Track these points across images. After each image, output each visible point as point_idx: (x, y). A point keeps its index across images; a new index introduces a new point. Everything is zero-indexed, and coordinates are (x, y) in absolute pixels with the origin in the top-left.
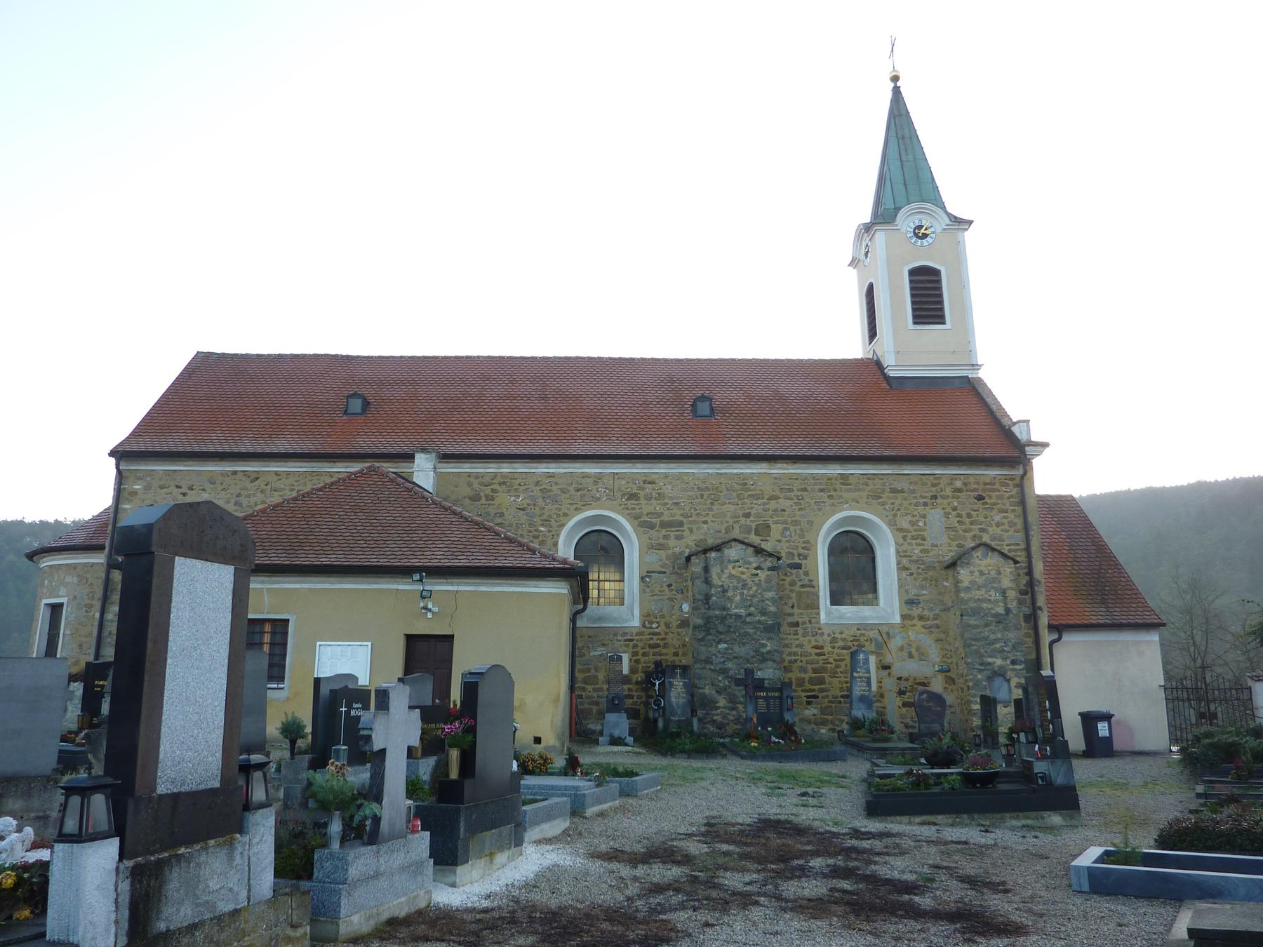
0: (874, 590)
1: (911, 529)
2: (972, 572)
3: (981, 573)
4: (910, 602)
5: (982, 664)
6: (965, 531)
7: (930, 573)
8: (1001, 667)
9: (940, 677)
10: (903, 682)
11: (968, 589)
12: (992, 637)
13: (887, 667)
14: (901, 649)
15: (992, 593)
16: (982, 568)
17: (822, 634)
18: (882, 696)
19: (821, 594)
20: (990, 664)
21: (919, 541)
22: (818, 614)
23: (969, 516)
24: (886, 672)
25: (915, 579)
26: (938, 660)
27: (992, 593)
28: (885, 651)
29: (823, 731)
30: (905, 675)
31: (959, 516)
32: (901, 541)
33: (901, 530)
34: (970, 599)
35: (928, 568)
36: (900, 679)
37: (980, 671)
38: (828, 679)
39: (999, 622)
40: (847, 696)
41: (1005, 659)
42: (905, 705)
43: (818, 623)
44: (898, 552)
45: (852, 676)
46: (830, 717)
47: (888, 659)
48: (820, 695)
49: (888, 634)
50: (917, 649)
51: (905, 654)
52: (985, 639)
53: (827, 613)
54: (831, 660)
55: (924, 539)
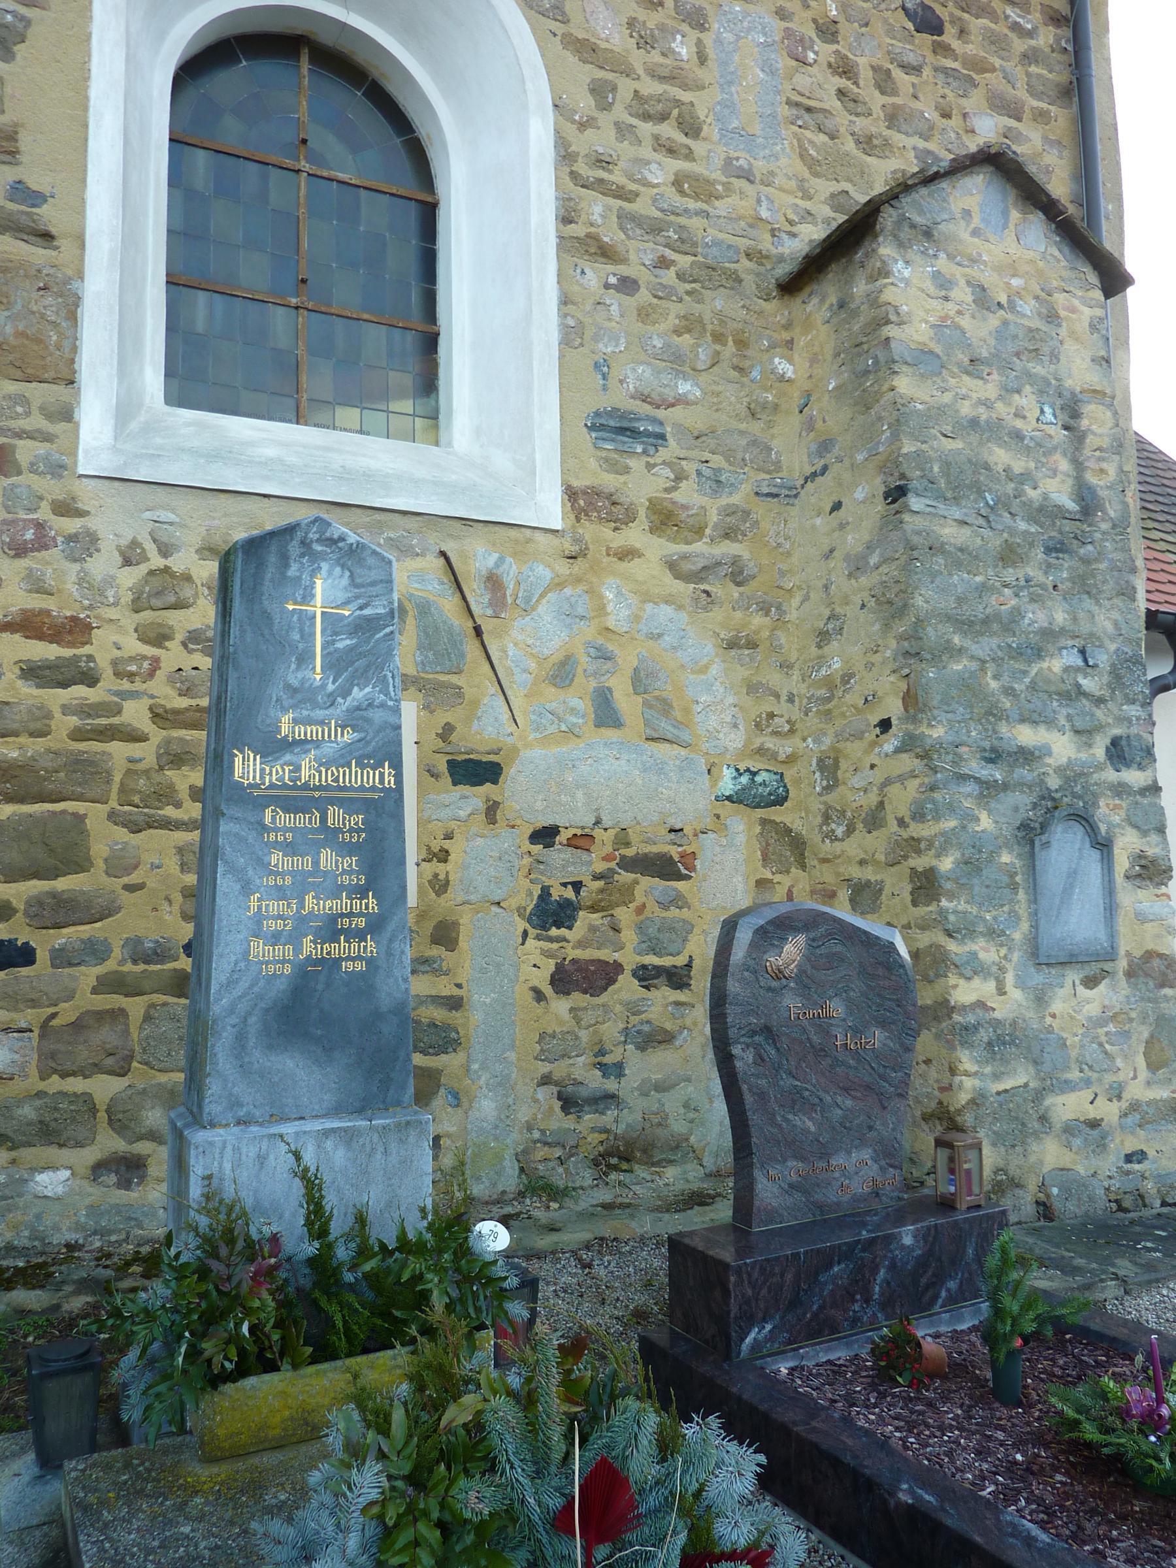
0: (428, 383)
1: (638, 59)
2: (943, 283)
3: (983, 299)
4: (619, 429)
5: (993, 756)
6: (867, 143)
7: (718, 302)
8: (1073, 775)
9: (742, 827)
10: (559, 855)
11: (927, 361)
12: (1035, 617)
13: (477, 771)
14: (561, 673)
15: (1027, 400)
16: (988, 277)
17: (83, 545)
18: (445, 934)
19: (98, 287)
20: (1026, 756)
21: (669, 131)
22: (66, 414)
23: (884, 82)
24: (474, 798)
25: (644, 314)
26: (734, 740)
27: (1027, 400)
28: (474, 679)
29: (51, 1182)
30: (572, 816)
31: (844, 69)
32: (585, 104)
33: (586, 50)
34: (938, 413)
35: (712, 275)
36: (545, 835)
37: (989, 790)
38: (104, 837)
39: (1056, 549)
40: (180, 985)
41: (1084, 734)
42: (566, 979)
43: (58, 470)
44: (565, 155)
45: (218, 792)
46: (104, 1088)
47: (487, 729)
48: (44, 943)
49: (493, 582)
50: (639, 682)
51: (577, 702)
52: (1010, 623)
53: (117, 403)
54: (135, 714)
55: (692, 129)
